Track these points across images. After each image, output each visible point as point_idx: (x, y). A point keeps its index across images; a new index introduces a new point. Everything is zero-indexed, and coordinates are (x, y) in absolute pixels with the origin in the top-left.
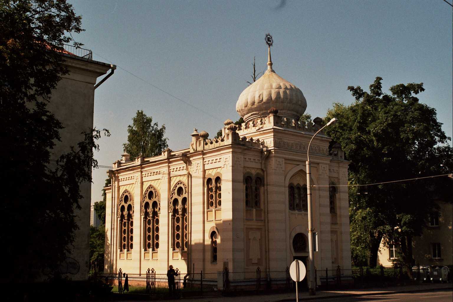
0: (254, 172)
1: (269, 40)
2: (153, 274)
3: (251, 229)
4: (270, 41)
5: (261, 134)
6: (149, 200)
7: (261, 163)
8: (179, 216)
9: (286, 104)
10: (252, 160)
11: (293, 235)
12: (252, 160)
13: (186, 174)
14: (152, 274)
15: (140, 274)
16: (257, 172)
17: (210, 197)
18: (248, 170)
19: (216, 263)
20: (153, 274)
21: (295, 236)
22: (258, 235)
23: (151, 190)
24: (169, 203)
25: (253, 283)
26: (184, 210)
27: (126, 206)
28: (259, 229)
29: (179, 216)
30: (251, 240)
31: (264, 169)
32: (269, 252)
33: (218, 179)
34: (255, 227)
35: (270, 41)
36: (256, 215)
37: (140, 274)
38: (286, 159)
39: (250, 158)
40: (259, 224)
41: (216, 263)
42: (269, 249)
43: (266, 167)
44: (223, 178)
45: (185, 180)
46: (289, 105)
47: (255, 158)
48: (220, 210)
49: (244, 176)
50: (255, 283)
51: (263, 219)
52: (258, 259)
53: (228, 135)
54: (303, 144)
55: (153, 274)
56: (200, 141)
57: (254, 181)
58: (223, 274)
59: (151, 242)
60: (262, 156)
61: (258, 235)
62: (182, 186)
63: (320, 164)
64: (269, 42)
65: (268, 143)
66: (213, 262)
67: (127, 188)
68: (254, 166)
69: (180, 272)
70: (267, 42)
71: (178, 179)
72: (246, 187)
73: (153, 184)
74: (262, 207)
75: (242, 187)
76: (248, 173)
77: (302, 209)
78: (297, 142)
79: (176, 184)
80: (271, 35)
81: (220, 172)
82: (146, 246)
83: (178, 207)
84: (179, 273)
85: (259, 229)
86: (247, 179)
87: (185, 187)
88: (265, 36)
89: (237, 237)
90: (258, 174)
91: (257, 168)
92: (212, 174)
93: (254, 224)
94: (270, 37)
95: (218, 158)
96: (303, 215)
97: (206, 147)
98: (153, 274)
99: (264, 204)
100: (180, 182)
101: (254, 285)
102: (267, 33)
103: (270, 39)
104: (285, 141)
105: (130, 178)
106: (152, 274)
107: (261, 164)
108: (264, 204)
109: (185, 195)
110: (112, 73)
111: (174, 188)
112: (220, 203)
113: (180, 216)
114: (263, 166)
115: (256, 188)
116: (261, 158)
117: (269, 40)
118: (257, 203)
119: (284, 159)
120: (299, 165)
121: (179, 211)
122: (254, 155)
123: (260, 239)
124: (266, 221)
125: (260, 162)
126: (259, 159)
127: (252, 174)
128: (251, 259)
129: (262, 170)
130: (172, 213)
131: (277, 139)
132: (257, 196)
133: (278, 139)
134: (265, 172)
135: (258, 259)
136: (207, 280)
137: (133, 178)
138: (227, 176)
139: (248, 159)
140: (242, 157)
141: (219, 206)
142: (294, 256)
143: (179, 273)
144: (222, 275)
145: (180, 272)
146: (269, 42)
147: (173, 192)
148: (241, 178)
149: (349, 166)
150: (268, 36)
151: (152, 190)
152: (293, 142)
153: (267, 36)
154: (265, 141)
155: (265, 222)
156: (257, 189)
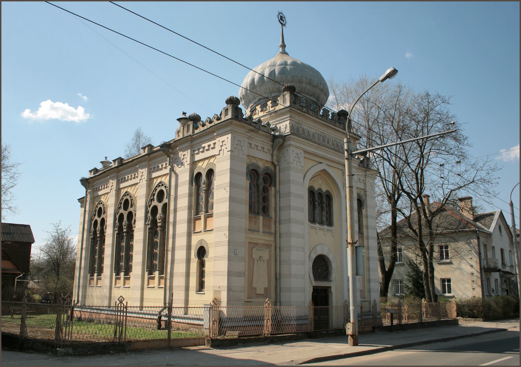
0: (261, 164)
1: (281, 19)
2: (122, 305)
3: (257, 244)
4: (283, 21)
7: (272, 154)
9: (304, 85)
11: (314, 256)
12: (259, 148)
14: (120, 305)
15: (109, 307)
16: (266, 165)
18: (254, 161)
20: (122, 305)
21: (315, 258)
22: (265, 254)
24: (147, 212)
26: (165, 220)
28: (268, 246)
31: (276, 163)
32: (280, 278)
33: (210, 173)
34: (263, 242)
35: (283, 21)
37: (109, 307)
42: (280, 274)
43: (278, 162)
44: (217, 171)
46: (308, 86)
47: (264, 146)
51: (273, 231)
53: (227, 109)
54: (327, 136)
55: (121, 307)
56: (188, 126)
57: (261, 177)
61: (265, 254)
62: (163, 188)
64: (282, 22)
65: (282, 127)
66: (200, 291)
68: (263, 157)
69: (127, 303)
71: (159, 180)
72: (250, 184)
74: (272, 213)
75: (245, 182)
76: (254, 164)
78: (319, 133)
79: (157, 187)
82: (117, 269)
84: (125, 305)
85: (268, 246)
86: (253, 173)
88: (277, 14)
90: (267, 168)
91: (267, 161)
92: (202, 167)
93: (261, 238)
95: (211, 143)
96: (326, 230)
97: (196, 131)
98: (121, 307)
99: (275, 211)
100: (161, 184)
102: (280, 12)
104: (305, 128)
106: (120, 305)
107: (272, 156)
108: (275, 211)
114: (275, 157)
115: (264, 187)
117: (281, 19)
118: (265, 210)
122: (262, 141)
123: (267, 261)
124: (278, 235)
126: (268, 148)
127: (258, 167)
128: (255, 289)
129: (273, 163)
131: (294, 123)
132: (266, 199)
133: (296, 122)
134: (277, 167)
136: (191, 316)
138: (223, 168)
140: (246, 140)
142: (314, 285)
143: (125, 305)
144: (163, 334)
145: (127, 303)
146: (282, 22)
148: (244, 169)
150: (281, 15)
151: (128, 197)
152: (314, 131)
154: (278, 126)
155: (275, 237)
156: (265, 190)
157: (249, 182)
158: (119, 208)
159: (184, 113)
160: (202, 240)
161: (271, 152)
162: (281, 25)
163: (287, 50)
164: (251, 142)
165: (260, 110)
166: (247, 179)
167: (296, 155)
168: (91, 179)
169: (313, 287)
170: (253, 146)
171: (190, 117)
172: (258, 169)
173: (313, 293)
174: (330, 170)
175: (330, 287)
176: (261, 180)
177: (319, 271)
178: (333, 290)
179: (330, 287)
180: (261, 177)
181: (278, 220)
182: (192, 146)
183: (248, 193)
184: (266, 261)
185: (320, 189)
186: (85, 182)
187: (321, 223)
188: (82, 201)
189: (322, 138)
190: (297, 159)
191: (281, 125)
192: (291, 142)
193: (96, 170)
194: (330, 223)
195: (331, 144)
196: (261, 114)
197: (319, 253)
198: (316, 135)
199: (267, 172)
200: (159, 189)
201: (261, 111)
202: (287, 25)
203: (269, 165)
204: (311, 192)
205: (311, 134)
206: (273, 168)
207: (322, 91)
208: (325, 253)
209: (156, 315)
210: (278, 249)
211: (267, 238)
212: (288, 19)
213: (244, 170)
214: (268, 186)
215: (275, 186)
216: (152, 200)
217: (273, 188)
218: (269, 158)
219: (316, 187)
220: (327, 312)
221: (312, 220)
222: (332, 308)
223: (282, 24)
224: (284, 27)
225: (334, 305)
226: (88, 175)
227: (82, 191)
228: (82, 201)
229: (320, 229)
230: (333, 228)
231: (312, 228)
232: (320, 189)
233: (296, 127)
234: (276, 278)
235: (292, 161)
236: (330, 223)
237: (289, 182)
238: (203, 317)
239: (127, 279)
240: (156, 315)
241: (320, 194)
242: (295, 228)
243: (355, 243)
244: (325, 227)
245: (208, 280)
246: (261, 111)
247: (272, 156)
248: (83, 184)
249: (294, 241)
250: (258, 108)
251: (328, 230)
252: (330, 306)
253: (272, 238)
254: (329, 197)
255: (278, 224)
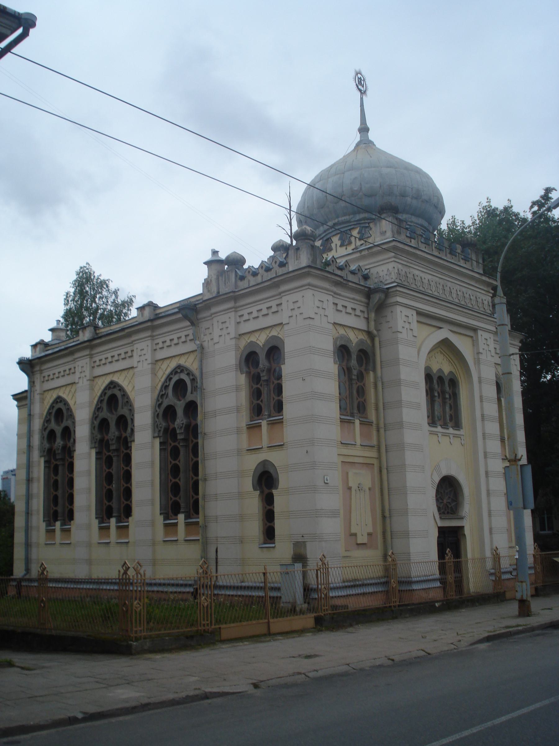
1: (360, 83)
4: (363, 86)
5: (363, 258)
6: (109, 414)
8: (176, 444)
10: (349, 310)
11: (437, 479)
13: (196, 350)
17: (256, 394)
19: (273, 545)
23: (114, 393)
25: (187, 589)
27: (58, 430)
29: (176, 444)
30: (353, 492)
31: (375, 332)
32: (390, 517)
35: (363, 86)
36: (361, 434)
38: (420, 313)
39: (346, 304)
40: (367, 454)
41: (273, 545)
45: (191, 363)
48: (281, 422)
49: (335, 340)
50: (380, 589)
51: (375, 442)
52: (369, 534)
57: (354, 356)
58: (317, 571)
59: (115, 503)
60: (368, 304)
62: (184, 376)
63: (479, 331)
64: (360, 87)
67: (61, 394)
70: (357, 87)
73: (120, 379)
74: (372, 415)
76: (342, 337)
77: (449, 425)
79: (171, 373)
80: (363, 74)
81: (280, 336)
82: (105, 512)
83: (176, 423)
87: (191, 377)
88: (353, 74)
89: (326, 482)
90: (361, 342)
94: (362, 79)
99: (377, 409)
101: (188, 592)
102: (358, 70)
103: (362, 82)
105: (67, 372)
107: (368, 322)
108: (377, 409)
109: (189, 397)
110: (24, 35)
111: (165, 384)
112: (279, 407)
113: (179, 443)
114: (372, 324)
116: (367, 307)
117: (360, 83)
118: (362, 408)
119: (414, 313)
120: (441, 328)
121: (178, 432)
122: (353, 299)
123: (370, 489)
125: (366, 316)
128: (355, 535)
130: (162, 438)
132: (361, 391)
134: (377, 340)
135: (369, 534)
137: (72, 371)
139: (343, 306)
140: (330, 298)
141: (277, 414)
146: (360, 87)
147: (163, 393)
149: (520, 342)
150: (359, 76)
153: (357, 74)
156: (361, 377)
157: (337, 366)
158: (99, 409)
159: (215, 253)
160: (265, 463)
161: (366, 316)
162: (359, 93)
163: (372, 136)
164: (336, 301)
165: (339, 243)
166: (335, 363)
167: (405, 319)
168: (36, 361)
169: (440, 528)
170: (340, 307)
171: (228, 258)
172: (348, 345)
173: (438, 537)
174: (456, 340)
175: (463, 527)
176: (354, 362)
177: (445, 501)
178: (467, 531)
179: (463, 527)
180: (354, 356)
181: (382, 425)
182: (236, 308)
183: (337, 383)
184: (367, 490)
185: (440, 370)
186: (26, 365)
187: (445, 426)
188: (20, 398)
189: (441, 287)
190: (407, 326)
191: (379, 269)
192: (399, 299)
193: (42, 343)
194: (457, 425)
195: (454, 296)
196: (342, 251)
197: (444, 473)
198: (432, 284)
199: (361, 348)
200: (175, 378)
201: (341, 246)
202: (368, 92)
203: (362, 336)
204: (429, 377)
205: (426, 281)
206: (369, 342)
207: (436, 207)
208: (453, 472)
209: (190, 585)
210: (384, 472)
211: (367, 454)
212: (369, 83)
213: (330, 347)
214: (363, 371)
215: (374, 370)
216: (163, 395)
217: (371, 373)
218: (361, 324)
219: (435, 368)
220: (458, 568)
221: (432, 422)
222: (467, 561)
223: (360, 90)
224: (364, 97)
225: (469, 555)
226: (28, 354)
227: (22, 382)
228: (20, 398)
229: (444, 435)
230: (462, 432)
231: (431, 433)
232: (440, 370)
233: (403, 273)
234: (384, 517)
235: (400, 329)
236: (457, 425)
237: (396, 362)
238: (279, 585)
239: (123, 529)
240: (190, 585)
241: (441, 379)
242: (410, 437)
243: (520, 460)
244: (451, 431)
245: (279, 525)
246: (341, 246)
247: (368, 322)
248: (23, 370)
249: (410, 457)
250: (336, 240)
251: (455, 436)
252: (463, 559)
253: (374, 454)
254: (453, 383)
255: (382, 431)
